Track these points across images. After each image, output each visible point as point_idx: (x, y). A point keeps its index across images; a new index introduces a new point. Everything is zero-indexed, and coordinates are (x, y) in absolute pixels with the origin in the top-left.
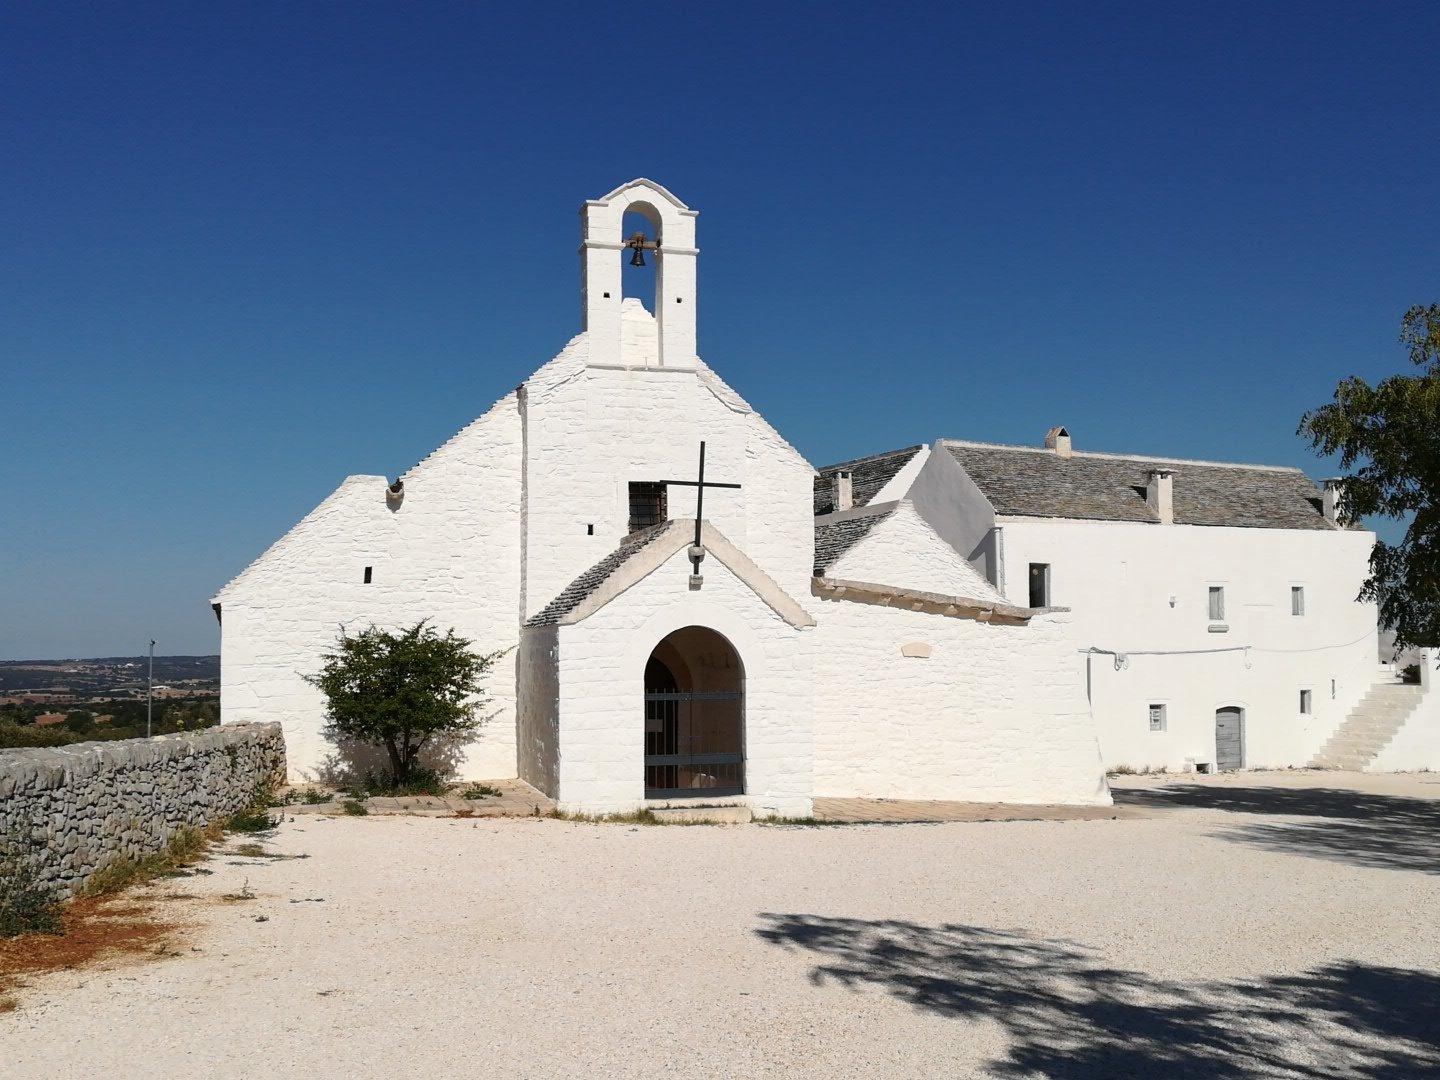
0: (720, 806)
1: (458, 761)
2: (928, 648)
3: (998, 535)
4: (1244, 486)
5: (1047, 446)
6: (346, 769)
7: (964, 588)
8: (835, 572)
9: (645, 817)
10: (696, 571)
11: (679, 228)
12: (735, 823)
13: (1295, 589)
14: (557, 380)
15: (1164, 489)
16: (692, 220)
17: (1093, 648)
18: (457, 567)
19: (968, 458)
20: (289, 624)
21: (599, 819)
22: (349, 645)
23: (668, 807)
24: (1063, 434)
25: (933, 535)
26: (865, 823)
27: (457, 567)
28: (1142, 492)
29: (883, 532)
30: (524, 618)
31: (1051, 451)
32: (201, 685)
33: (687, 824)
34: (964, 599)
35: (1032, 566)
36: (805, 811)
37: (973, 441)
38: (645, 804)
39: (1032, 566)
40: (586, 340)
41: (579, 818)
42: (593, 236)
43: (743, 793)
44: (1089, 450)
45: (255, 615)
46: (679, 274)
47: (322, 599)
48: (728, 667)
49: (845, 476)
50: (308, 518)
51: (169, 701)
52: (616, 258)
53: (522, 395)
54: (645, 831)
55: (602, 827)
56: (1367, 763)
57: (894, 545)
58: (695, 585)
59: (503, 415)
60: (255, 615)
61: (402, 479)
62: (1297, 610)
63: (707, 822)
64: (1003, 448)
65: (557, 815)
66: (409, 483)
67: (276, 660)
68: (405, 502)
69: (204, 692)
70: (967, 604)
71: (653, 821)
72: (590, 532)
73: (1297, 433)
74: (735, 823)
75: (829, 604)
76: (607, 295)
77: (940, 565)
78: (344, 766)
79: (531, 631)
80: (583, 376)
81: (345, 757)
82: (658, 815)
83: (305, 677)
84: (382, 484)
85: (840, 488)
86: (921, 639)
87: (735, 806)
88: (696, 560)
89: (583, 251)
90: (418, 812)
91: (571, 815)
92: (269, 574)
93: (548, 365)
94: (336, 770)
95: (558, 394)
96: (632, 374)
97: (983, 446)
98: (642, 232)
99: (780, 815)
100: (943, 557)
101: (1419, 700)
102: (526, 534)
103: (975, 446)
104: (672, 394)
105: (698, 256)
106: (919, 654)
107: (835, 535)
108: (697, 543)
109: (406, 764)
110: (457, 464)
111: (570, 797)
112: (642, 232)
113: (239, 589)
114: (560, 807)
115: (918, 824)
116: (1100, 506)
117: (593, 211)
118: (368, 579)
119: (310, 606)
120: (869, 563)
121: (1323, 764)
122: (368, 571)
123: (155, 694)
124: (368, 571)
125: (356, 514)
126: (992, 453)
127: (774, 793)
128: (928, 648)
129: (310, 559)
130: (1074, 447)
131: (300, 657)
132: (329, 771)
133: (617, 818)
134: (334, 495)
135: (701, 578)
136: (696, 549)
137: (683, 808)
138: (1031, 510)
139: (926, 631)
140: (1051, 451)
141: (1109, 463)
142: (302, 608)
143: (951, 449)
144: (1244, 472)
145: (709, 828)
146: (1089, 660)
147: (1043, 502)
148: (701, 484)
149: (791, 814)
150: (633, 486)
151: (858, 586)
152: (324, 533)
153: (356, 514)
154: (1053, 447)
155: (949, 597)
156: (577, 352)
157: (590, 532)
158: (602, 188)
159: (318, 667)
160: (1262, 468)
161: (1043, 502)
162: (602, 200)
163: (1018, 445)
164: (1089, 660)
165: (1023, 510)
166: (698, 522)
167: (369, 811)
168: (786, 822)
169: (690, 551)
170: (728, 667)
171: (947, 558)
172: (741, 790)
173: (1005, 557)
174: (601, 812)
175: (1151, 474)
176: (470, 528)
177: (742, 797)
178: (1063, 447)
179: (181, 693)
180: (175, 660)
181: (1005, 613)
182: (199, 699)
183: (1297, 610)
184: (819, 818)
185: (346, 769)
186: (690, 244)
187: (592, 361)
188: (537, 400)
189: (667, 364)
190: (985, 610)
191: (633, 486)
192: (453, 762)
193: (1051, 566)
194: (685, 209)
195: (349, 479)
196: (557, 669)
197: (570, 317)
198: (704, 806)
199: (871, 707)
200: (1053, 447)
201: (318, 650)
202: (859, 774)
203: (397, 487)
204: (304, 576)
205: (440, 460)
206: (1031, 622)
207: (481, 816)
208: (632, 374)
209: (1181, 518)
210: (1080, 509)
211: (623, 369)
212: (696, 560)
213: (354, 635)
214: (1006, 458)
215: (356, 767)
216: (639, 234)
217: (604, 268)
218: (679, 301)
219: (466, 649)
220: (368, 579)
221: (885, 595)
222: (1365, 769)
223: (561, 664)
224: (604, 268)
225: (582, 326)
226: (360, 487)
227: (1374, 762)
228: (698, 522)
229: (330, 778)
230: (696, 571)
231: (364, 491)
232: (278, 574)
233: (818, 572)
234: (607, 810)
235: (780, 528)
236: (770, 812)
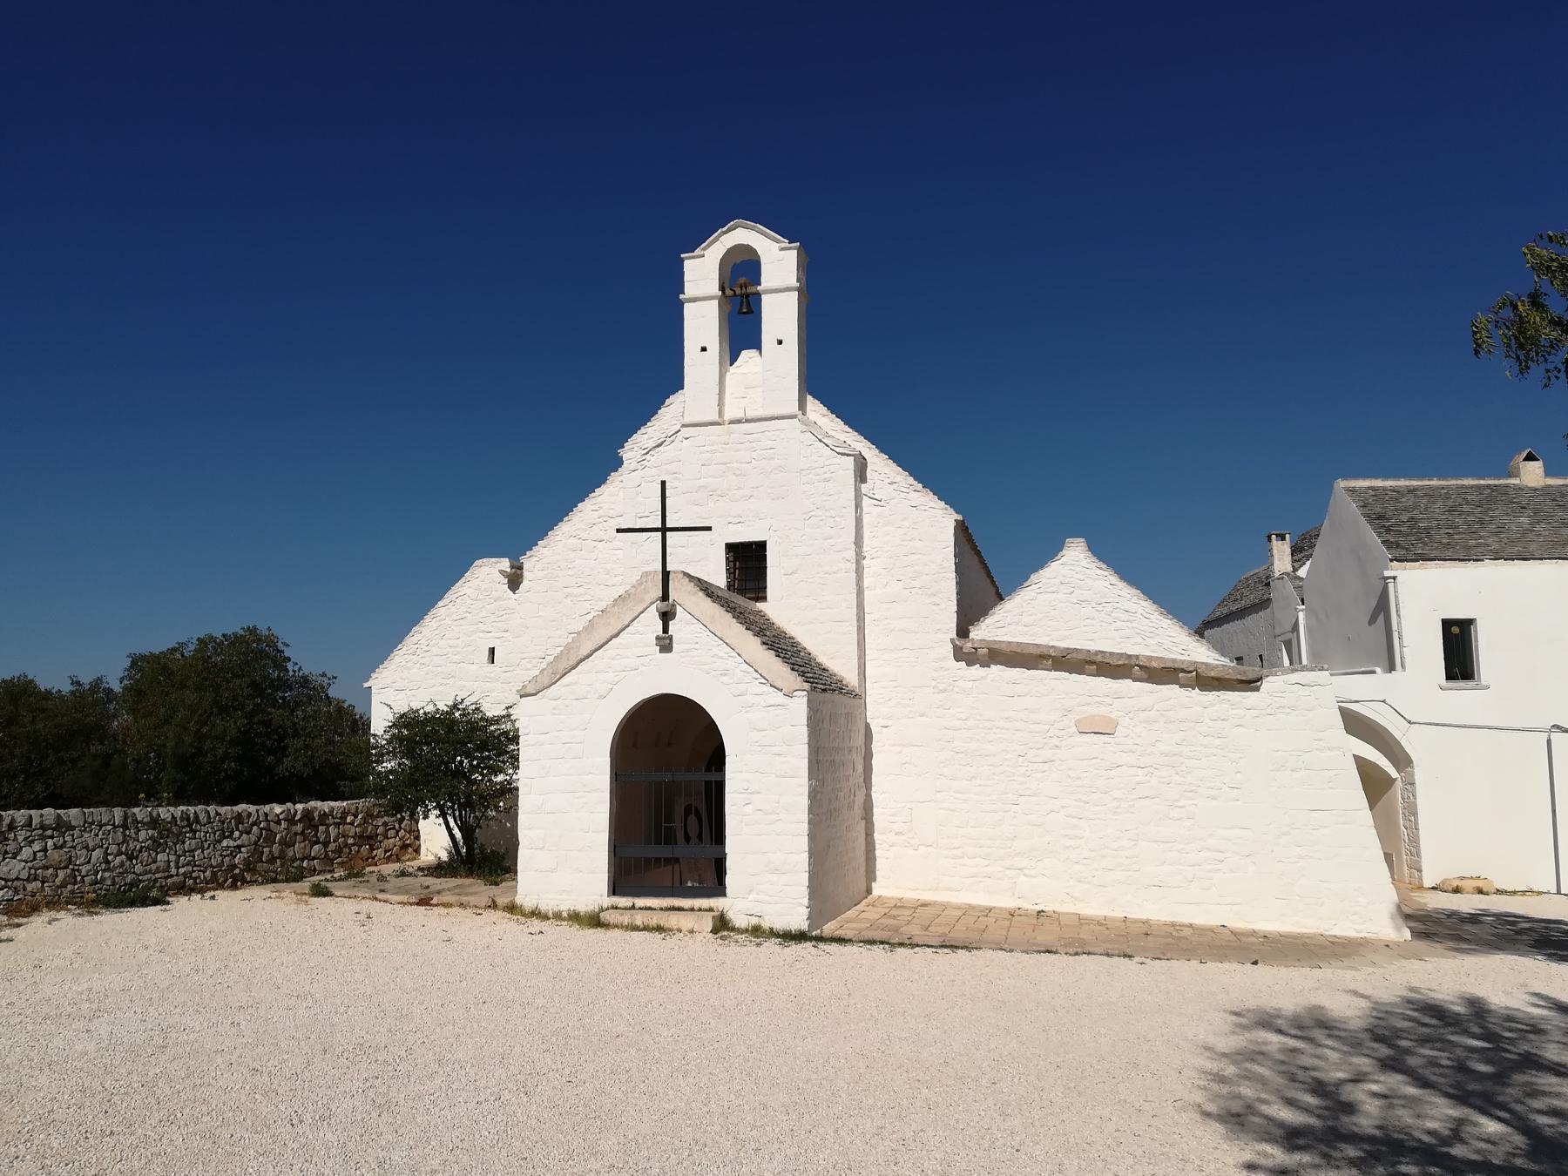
0: (692, 910)
3: (1391, 586)
5: (1510, 476)
7: (1160, 644)
8: (980, 633)
10: (665, 630)
11: (780, 264)
12: (692, 932)
14: (651, 444)
16: (795, 252)
17: (1558, 727)
23: (633, 907)
24: (1530, 458)
25: (1114, 579)
26: (954, 947)
29: (1044, 580)
33: (636, 928)
34: (1150, 658)
35: (1447, 624)
37: (1386, 477)
38: (608, 901)
39: (1447, 624)
41: (536, 914)
42: (690, 289)
46: (781, 315)
49: (1282, 537)
50: (440, 604)
52: (712, 308)
57: (1060, 596)
58: (665, 644)
63: (659, 929)
70: (1154, 664)
73: (1477, 352)
75: (976, 670)
76: (704, 349)
77: (1125, 616)
84: (505, 564)
85: (1275, 552)
86: (1104, 710)
88: (666, 617)
89: (680, 306)
90: (380, 896)
93: (643, 430)
95: (652, 459)
96: (740, 431)
100: (1127, 605)
103: (1390, 483)
104: (770, 444)
105: (799, 290)
106: (1101, 729)
107: (982, 582)
110: (573, 540)
113: (385, 673)
115: (878, 950)
120: (1026, 619)
122: (492, 651)
124: (492, 651)
127: (761, 897)
129: (442, 642)
130: (1548, 473)
135: (671, 638)
137: (650, 908)
138: (1449, 553)
139: (1108, 700)
143: (1352, 491)
146: (1549, 741)
147: (1473, 542)
148: (664, 530)
149: (780, 924)
150: (761, 546)
151: (1003, 646)
154: (1517, 475)
155: (1130, 656)
158: (696, 239)
161: (1473, 542)
162: (698, 252)
164: (1549, 741)
165: (1434, 554)
171: (1132, 607)
173: (1402, 613)
177: (721, 900)
178: (1532, 474)
181: (1213, 674)
187: (687, 420)
188: (632, 467)
190: (1183, 671)
191: (761, 546)
193: (1479, 622)
194: (785, 243)
199: (1035, 795)
200: (1517, 475)
202: (1023, 878)
206: (1266, 685)
208: (740, 431)
210: (1532, 547)
212: (666, 617)
214: (1431, 494)
217: (702, 323)
221: (1043, 657)
225: (679, 385)
226: (485, 569)
231: (488, 573)
233: (963, 632)
234: (565, 907)
235: (915, 584)
236: (754, 921)
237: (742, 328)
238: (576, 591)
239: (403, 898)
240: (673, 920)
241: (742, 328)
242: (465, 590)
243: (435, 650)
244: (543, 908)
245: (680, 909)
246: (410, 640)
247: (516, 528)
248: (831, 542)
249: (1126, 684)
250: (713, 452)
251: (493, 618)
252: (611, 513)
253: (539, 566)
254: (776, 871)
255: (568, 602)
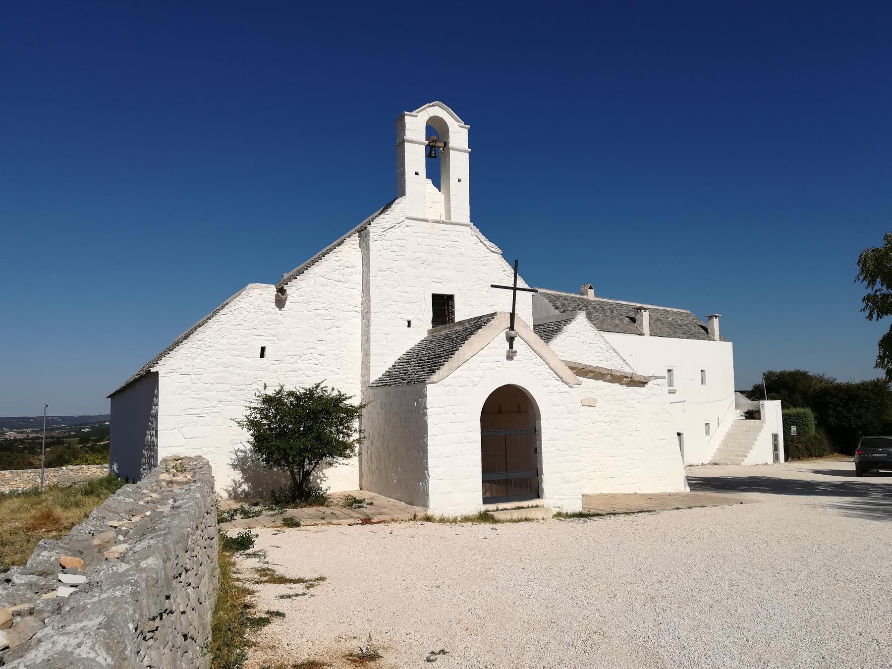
1: (321, 480)
2: (595, 401)
4: (671, 318)
6: (247, 489)
9: (485, 517)
10: (511, 347)
11: (458, 135)
13: (702, 371)
14: (388, 226)
15: (646, 315)
18: (321, 348)
19: (551, 298)
20: (208, 386)
21: (455, 521)
22: (267, 400)
23: (497, 510)
24: (591, 288)
26: (614, 514)
27: (321, 348)
28: (633, 320)
30: (368, 381)
31: (585, 297)
32: (33, 432)
33: (515, 521)
34: (616, 371)
36: (578, 508)
37: (550, 289)
38: (483, 508)
40: (405, 201)
41: (442, 520)
42: (408, 135)
43: (539, 497)
44: (602, 297)
45: (182, 380)
46: (459, 164)
47: (231, 369)
48: (500, 412)
51: (15, 440)
53: (363, 233)
54: (486, 527)
55: (458, 528)
56: (743, 461)
58: (510, 357)
59: (349, 250)
60: (182, 380)
61: (285, 287)
62: (703, 382)
63: (526, 520)
64: (564, 294)
65: (428, 519)
66: (290, 289)
67: (198, 411)
68: (287, 303)
69: (35, 435)
71: (494, 520)
72: (409, 326)
74: (543, 519)
76: (417, 174)
77: (600, 350)
78: (245, 487)
79: (371, 391)
80: (404, 224)
81: (247, 480)
82: (497, 515)
83: (239, 423)
84: (272, 290)
87: (537, 506)
88: (511, 340)
90: (335, 521)
91: (438, 519)
92: (194, 351)
94: (240, 490)
97: (555, 292)
98: (436, 138)
99: (564, 512)
101: (762, 427)
102: (368, 326)
104: (457, 239)
105: (470, 154)
108: (512, 327)
109: (301, 483)
111: (437, 505)
112: (436, 138)
113: (171, 361)
114: (430, 513)
116: (616, 326)
117: (408, 119)
118: (262, 356)
119: (222, 374)
121: (717, 462)
123: (7, 437)
125: (254, 310)
126: (560, 296)
128: (595, 401)
129: (222, 341)
130: (596, 296)
131: (215, 410)
132: (234, 490)
133: (467, 519)
134: (240, 297)
136: (512, 332)
137: (506, 509)
140: (585, 297)
141: (612, 304)
142: (216, 374)
144: (667, 311)
145: (529, 523)
149: (570, 510)
150: (435, 297)
152: (233, 322)
153: (254, 310)
154: (586, 294)
156: (400, 207)
157: (409, 326)
158: (414, 105)
159: (242, 412)
160: (675, 310)
162: (414, 113)
163: (571, 292)
166: (512, 315)
167: (302, 523)
168: (568, 516)
169: (507, 334)
170: (500, 412)
172: (537, 493)
174: (456, 515)
175: (639, 309)
176: (330, 322)
178: (591, 295)
179: (121, 436)
180: (19, 419)
182: (33, 439)
183: (703, 382)
184: (586, 512)
185: (247, 489)
186: (465, 145)
188: (376, 237)
189: (453, 220)
190: (627, 377)
192: (318, 481)
195: (250, 285)
196: (425, 414)
197: (391, 189)
198: (519, 508)
200: (586, 294)
201: (243, 404)
203: (281, 291)
204: (219, 352)
205: (310, 276)
207: (379, 522)
209: (653, 333)
211: (427, 221)
212: (511, 340)
213: (270, 392)
215: (254, 487)
216: (434, 137)
217: (415, 157)
218: (459, 180)
219: (347, 402)
220: (262, 356)
222: (743, 464)
223: (429, 411)
224: (415, 157)
225: (401, 192)
227: (746, 460)
228: (512, 315)
229: (235, 496)
230: (511, 347)
231: (260, 294)
232: (199, 351)
237: (436, 168)
238: (324, 313)
239: (352, 521)
240: (523, 514)
241: (436, 168)
242: (241, 304)
243: (218, 346)
244: (446, 515)
245: (523, 508)
246: (199, 336)
247: (282, 262)
248: (488, 300)
249: (600, 383)
250: (423, 237)
251: (264, 326)
252: (348, 264)
253: (298, 293)
254: (568, 482)
255: (317, 319)
